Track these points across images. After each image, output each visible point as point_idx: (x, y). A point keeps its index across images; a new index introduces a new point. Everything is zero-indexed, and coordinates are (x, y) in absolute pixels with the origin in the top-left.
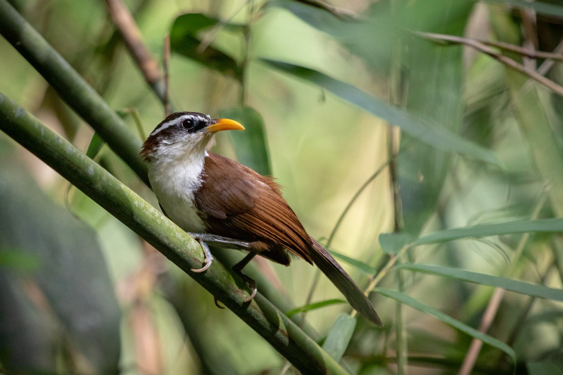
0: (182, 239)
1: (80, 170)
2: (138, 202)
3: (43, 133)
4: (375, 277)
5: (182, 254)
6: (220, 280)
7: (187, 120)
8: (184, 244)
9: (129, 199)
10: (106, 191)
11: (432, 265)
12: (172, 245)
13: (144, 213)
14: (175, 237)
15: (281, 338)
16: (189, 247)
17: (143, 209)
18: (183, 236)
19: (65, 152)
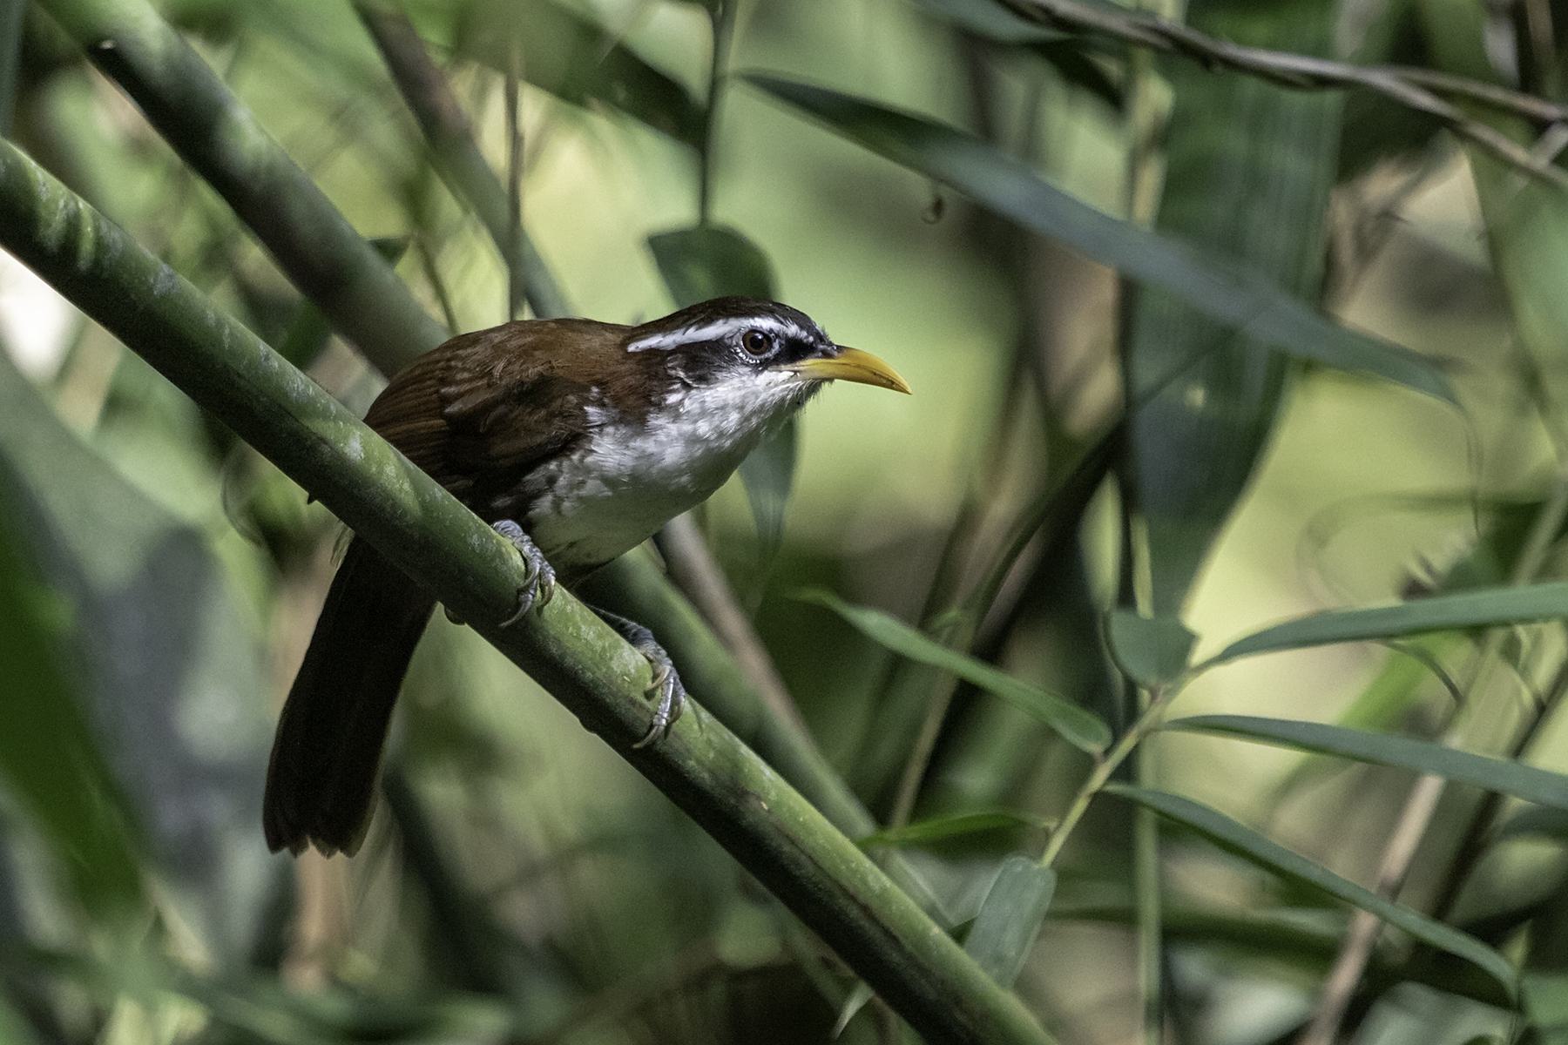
0: (599, 645)
1: (326, 449)
2: (480, 537)
3: (227, 342)
4: (1107, 752)
5: (597, 687)
6: (699, 761)
7: (754, 330)
8: (603, 658)
9: (776, 841)
10: (393, 506)
11: (487, 396)
12: (569, 661)
13: (495, 568)
14: (578, 638)
15: (860, 927)
16: (615, 666)
17: (493, 560)
18: (600, 636)
19: (286, 394)
